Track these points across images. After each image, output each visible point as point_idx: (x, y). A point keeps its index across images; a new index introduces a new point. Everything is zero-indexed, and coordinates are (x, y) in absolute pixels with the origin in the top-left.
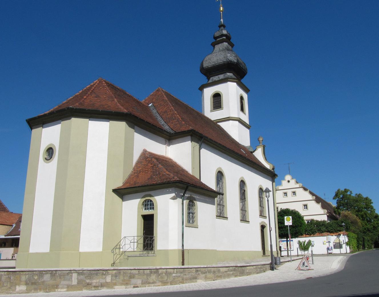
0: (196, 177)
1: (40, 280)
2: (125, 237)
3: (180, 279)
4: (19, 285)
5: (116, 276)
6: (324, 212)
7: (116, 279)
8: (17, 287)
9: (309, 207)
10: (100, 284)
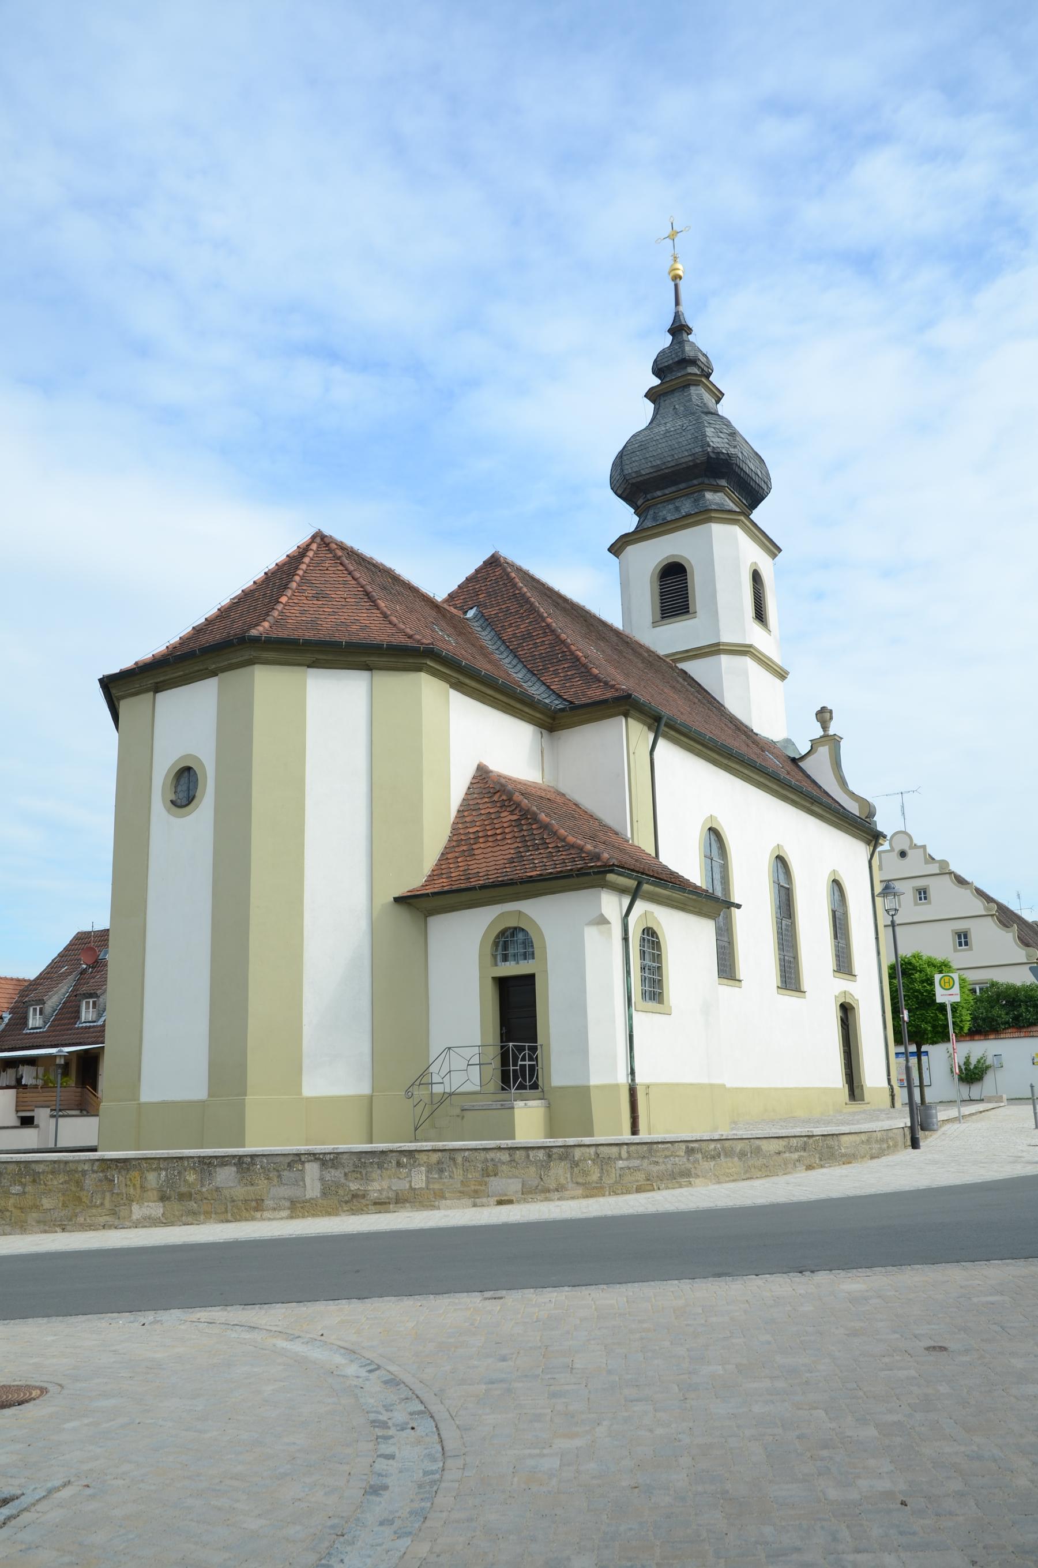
0: (648, 851)
2: (449, 1048)
3: (640, 1176)
4: (141, 1200)
8: (135, 1207)
9: (974, 938)
10: (392, 1195)
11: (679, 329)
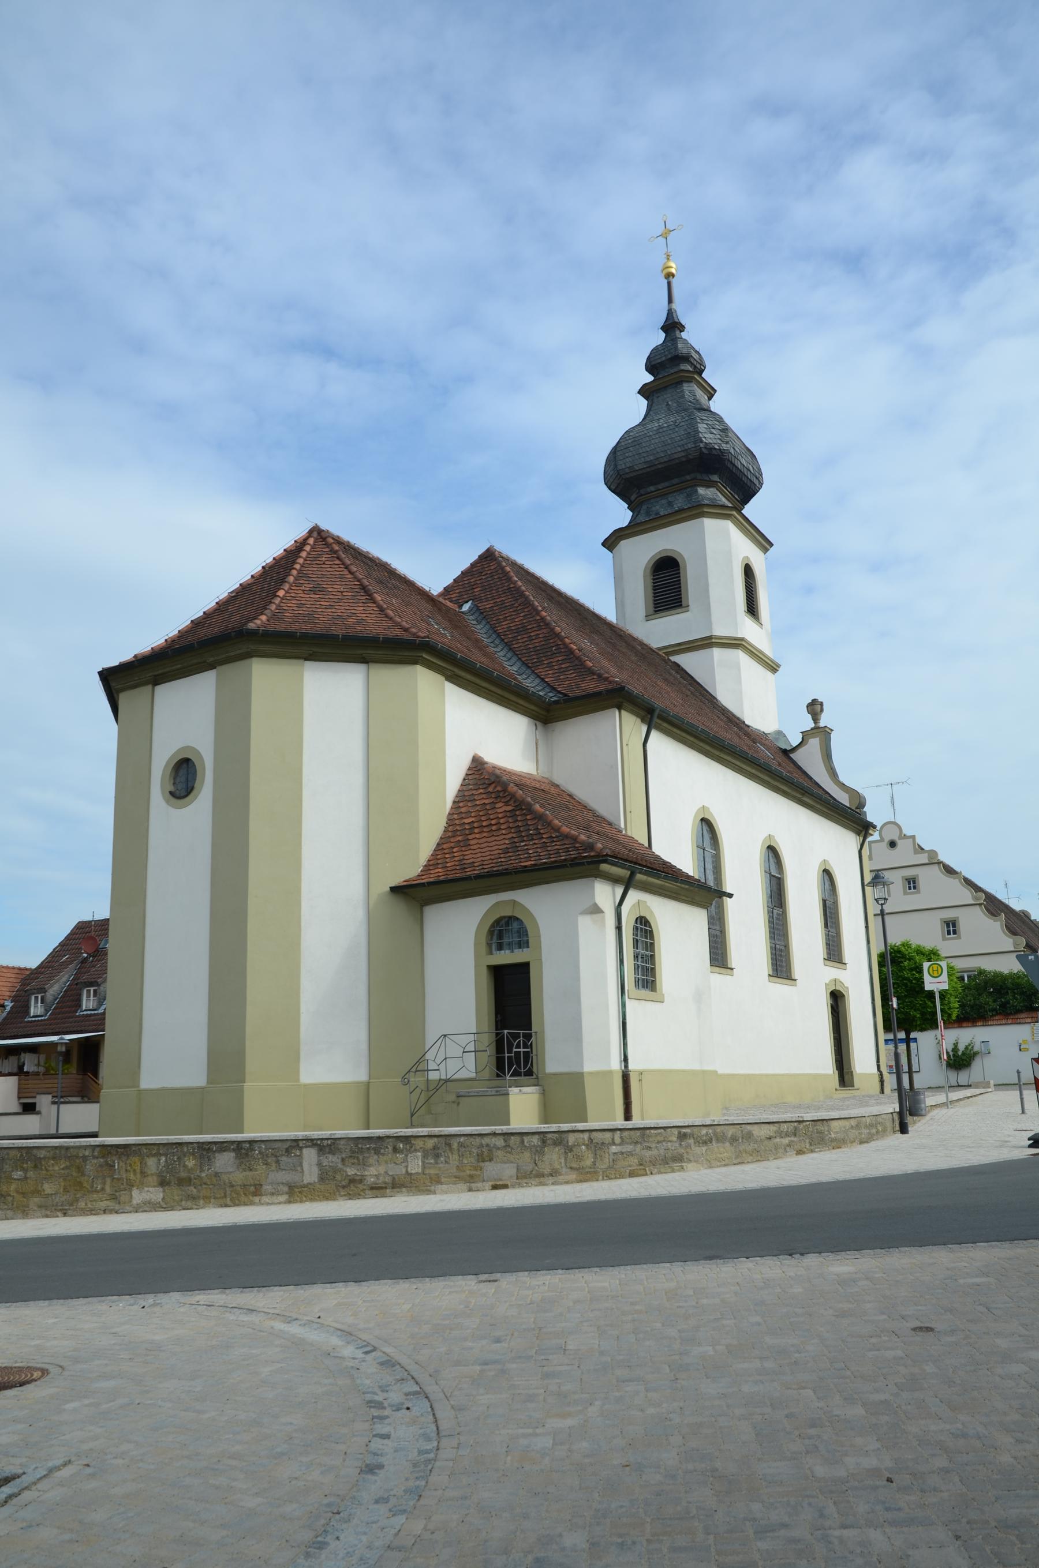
1: (202, 1171)
2: (445, 1036)
3: (634, 1161)
4: (141, 1185)
5: (437, 1156)
6: (1015, 944)
7: (437, 1163)
8: (135, 1192)
10: (388, 1179)
11: (672, 326)
